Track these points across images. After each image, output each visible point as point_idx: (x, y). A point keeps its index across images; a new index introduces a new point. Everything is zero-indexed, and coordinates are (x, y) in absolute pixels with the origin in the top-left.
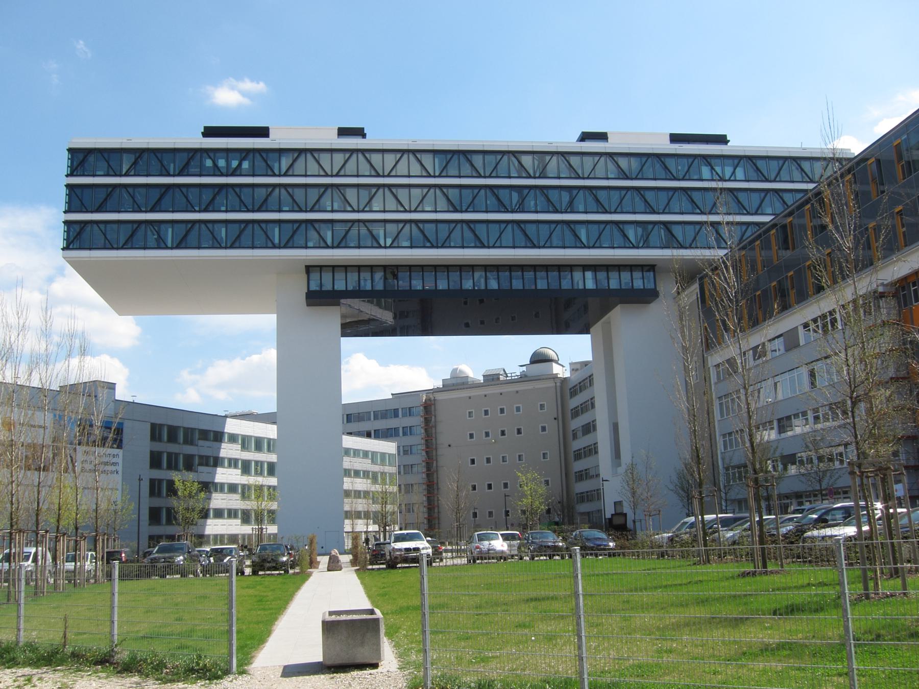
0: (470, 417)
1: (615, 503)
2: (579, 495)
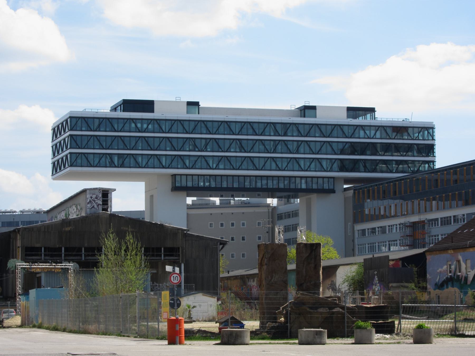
0: (210, 227)
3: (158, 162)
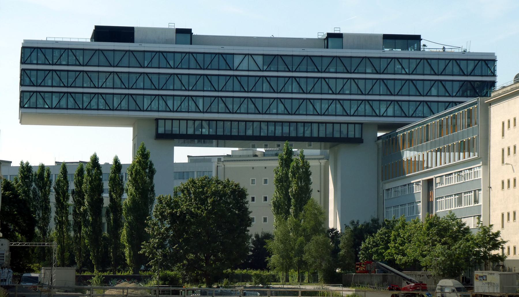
3: (429, 110)
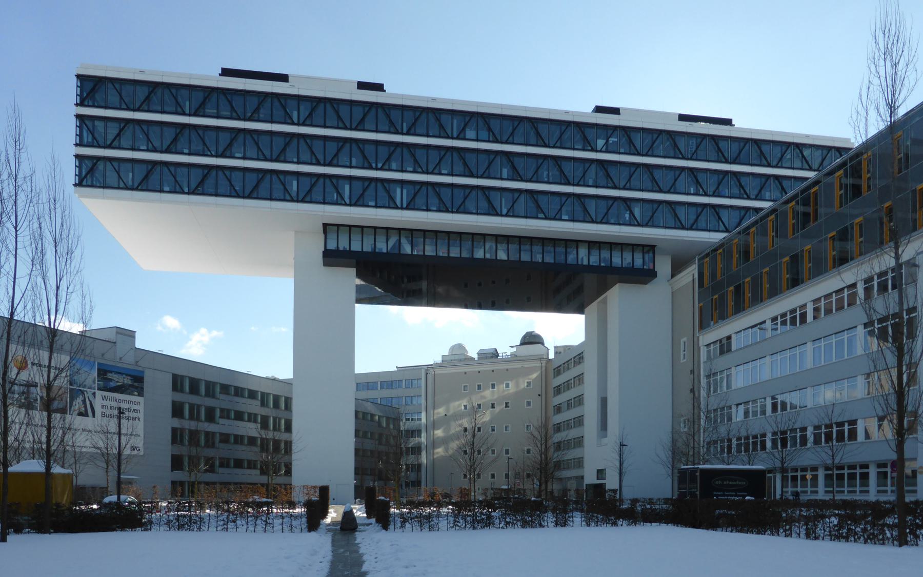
1: (598, 471)
2: (576, 460)
